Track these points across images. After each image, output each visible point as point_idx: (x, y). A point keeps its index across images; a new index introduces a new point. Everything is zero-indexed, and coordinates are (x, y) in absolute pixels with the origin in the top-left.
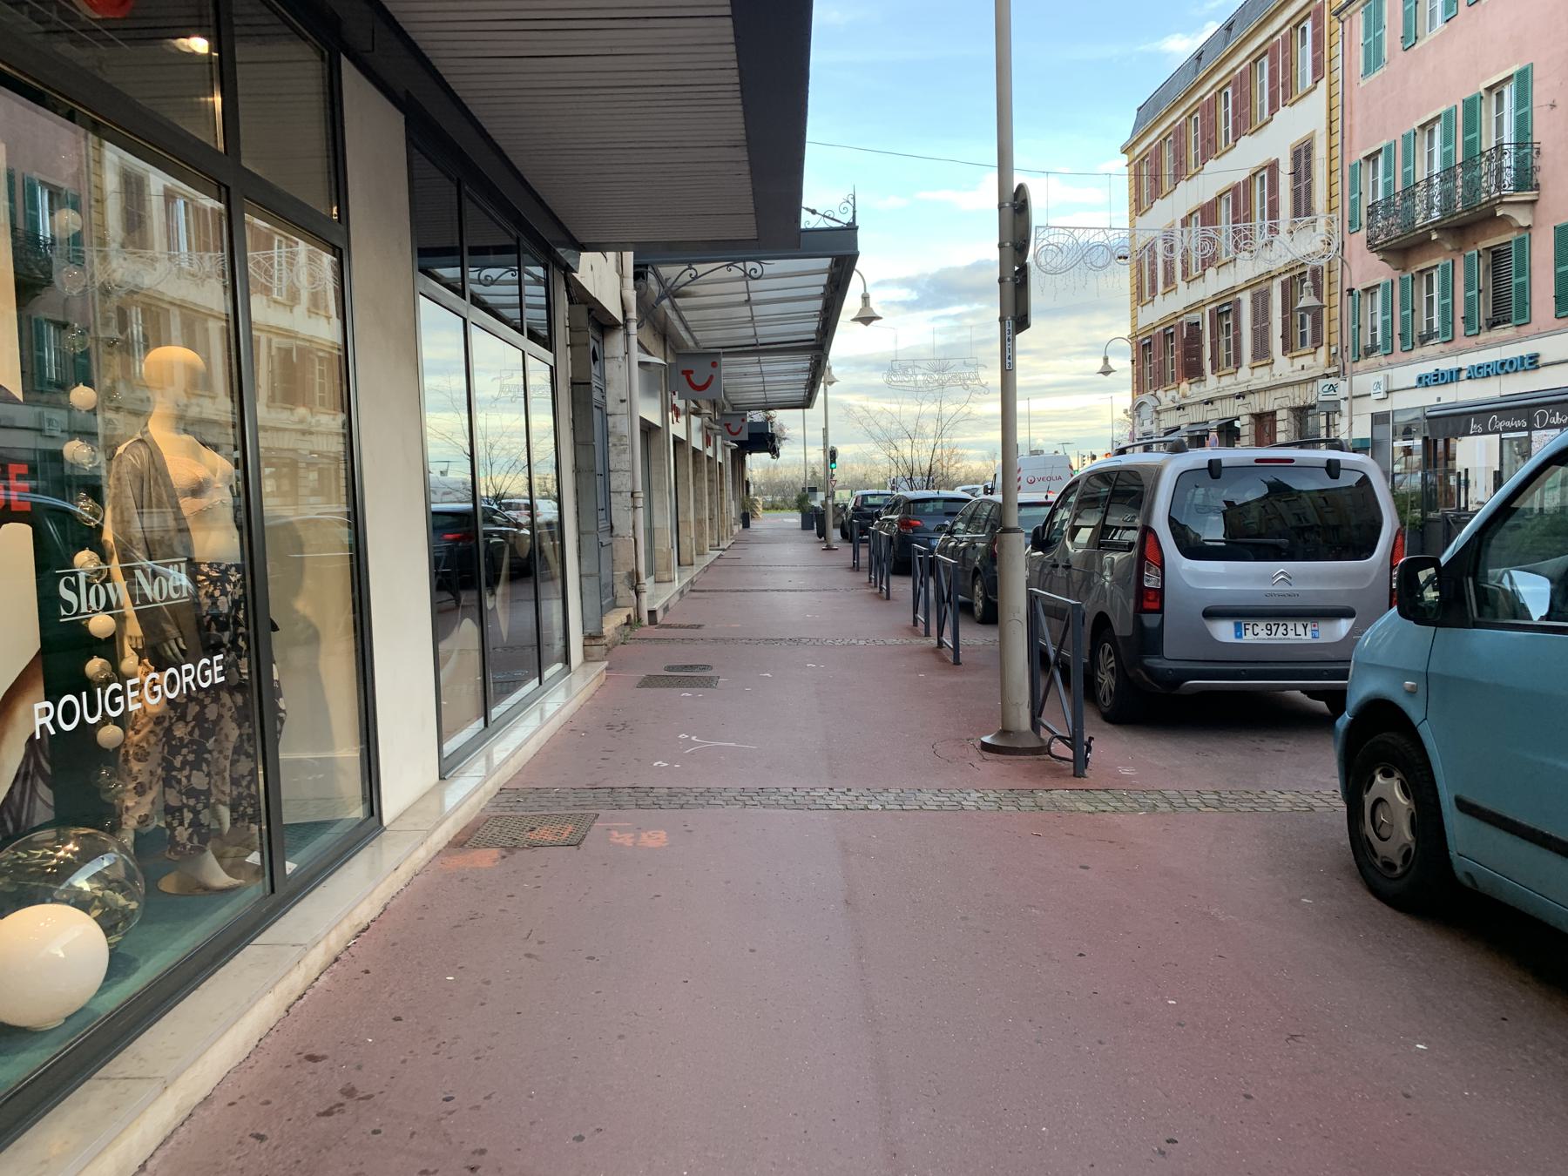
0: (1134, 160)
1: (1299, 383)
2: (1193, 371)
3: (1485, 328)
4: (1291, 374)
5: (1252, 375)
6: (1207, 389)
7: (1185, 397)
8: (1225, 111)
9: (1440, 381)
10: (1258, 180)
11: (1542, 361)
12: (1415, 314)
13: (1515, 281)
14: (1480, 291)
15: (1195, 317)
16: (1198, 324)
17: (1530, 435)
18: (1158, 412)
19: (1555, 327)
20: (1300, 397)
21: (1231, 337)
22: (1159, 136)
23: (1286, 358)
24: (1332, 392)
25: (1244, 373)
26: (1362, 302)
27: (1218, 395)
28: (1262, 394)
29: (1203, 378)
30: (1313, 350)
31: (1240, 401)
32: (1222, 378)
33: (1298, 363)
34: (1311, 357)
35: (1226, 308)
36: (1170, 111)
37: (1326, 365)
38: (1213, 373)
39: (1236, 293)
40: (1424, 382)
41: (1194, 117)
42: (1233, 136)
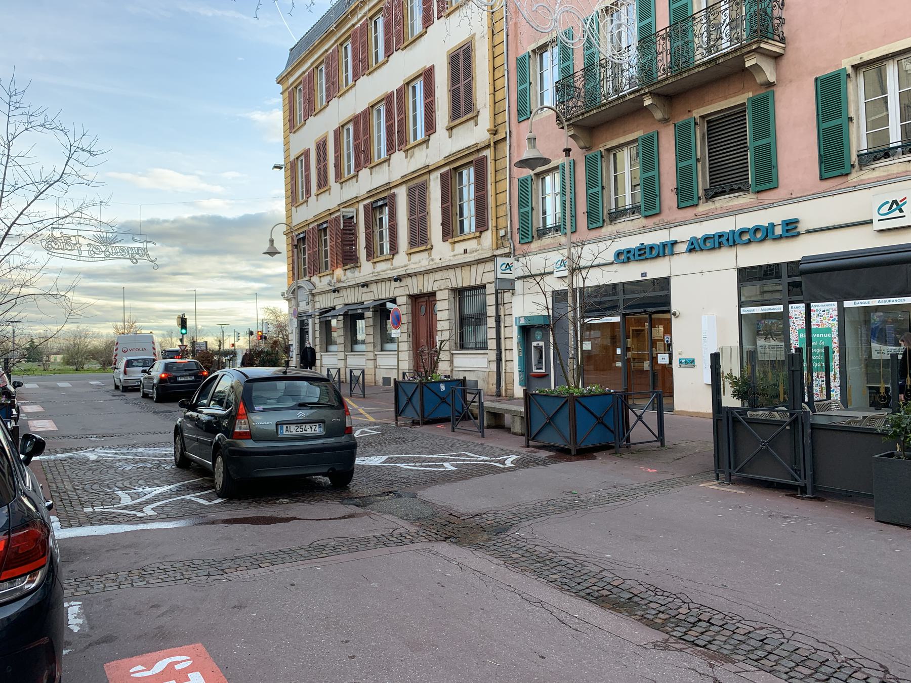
0: (288, 88)
1: (462, 265)
2: (349, 259)
3: (607, 221)
4: (452, 258)
5: (409, 260)
6: (361, 274)
7: (339, 281)
8: (321, 82)
9: (648, 255)
10: (375, 113)
11: (802, 228)
12: (604, 191)
13: (324, 260)
14: (698, 160)
15: (350, 212)
16: (352, 217)
17: (786, 309)
18: (313, 295)
19: (819, 190)
20: (416, 286)
21: (328, 248)
22: (312, 64)
23: (447, 243)
24: (508, 271)
25: (401, 259)
26: (534, 186)
27: (374, 278)
28: (420, 278)
29: (359, 265)
30: (478, 234)
31: (397, 284)
32: (377, 264)
33: (460, 248)
34: (475, 241)
35: (381, 203)
36: (322, 42)
37: (495, 247)
39: (390, 188)
40: (625, 257)
41: (298, 88)
42: (304, 117)
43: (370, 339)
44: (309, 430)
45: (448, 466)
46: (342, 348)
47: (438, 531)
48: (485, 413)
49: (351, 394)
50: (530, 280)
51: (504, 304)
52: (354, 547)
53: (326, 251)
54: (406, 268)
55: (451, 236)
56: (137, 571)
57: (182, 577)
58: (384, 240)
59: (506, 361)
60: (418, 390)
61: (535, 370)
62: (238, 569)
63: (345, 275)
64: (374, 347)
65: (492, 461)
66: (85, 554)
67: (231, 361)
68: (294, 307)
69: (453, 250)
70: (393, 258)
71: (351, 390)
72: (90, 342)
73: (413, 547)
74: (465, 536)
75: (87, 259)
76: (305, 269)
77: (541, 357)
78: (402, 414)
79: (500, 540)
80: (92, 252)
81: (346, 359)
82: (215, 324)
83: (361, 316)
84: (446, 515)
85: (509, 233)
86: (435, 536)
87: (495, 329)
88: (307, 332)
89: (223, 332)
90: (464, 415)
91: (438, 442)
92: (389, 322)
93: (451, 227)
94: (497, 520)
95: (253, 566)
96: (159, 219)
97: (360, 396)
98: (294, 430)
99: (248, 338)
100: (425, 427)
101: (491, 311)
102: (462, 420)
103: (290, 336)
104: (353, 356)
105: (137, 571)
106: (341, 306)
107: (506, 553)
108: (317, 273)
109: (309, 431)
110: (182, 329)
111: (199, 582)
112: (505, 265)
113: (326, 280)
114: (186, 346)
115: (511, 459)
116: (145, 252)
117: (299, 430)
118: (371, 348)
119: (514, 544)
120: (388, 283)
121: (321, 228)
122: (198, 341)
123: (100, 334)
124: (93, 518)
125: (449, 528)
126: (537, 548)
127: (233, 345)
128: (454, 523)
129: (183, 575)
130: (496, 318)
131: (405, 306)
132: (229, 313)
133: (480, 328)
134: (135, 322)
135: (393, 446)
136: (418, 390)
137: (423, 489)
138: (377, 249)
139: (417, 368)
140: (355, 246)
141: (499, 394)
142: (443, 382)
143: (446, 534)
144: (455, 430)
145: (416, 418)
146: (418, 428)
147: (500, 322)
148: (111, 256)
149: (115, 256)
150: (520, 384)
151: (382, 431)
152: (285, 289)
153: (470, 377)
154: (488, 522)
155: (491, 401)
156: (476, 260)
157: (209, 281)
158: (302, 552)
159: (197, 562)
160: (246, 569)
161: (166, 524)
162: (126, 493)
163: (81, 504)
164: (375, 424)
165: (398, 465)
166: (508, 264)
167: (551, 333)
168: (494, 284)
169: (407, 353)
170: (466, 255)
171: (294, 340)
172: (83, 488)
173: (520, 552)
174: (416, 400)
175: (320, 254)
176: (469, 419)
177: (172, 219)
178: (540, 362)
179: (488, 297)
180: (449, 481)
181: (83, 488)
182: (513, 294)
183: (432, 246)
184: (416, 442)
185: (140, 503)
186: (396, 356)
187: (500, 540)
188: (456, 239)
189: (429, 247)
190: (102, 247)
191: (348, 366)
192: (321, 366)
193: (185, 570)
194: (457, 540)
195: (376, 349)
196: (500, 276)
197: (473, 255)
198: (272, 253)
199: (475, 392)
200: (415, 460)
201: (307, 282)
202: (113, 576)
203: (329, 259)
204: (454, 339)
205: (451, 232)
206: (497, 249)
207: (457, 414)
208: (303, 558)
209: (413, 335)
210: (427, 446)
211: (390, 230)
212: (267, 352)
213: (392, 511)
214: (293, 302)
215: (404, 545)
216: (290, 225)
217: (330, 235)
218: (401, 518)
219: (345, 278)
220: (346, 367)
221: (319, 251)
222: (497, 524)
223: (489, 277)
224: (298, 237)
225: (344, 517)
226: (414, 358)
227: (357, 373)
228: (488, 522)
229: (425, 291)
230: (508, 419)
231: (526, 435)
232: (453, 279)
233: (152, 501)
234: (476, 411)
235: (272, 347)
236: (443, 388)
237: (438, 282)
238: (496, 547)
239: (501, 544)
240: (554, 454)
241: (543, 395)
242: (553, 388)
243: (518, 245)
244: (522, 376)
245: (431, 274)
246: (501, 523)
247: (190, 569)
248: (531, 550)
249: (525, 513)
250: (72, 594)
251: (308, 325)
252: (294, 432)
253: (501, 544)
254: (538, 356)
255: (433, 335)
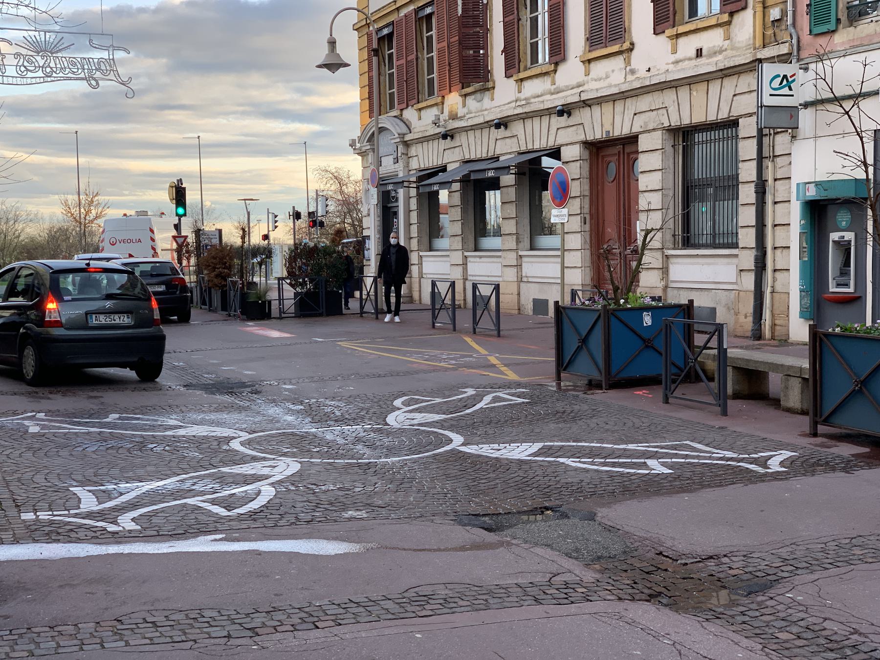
5: (587, 74)
6: (496, 103)
7: (454, 117)
13: (426, 77)
18: (407, 144)
21: (434, 54)
23: (662, 38)
24: (786, 91)
27: (519, 111)
28: (607, 108)
29: (490, 85)
30: (725, 18)
31: (563, 120)
33: (687, 46)
34: (719, 33)
37: (759, 43)
38: (508, 76)
43: (509, 227)
44: (118, 320)
45: (656, 466)
46: (457, 243)
47: (635, 583)
48: (730, 370)
49: (474, 329)
50: (830, 107)
51: (774, 156)
52: (482, 602)
53: (430, 61)
54: (581, 89)
55: (671, 22)
56: (110, 623)
57: (184, 638)
58: (540, 35)
59: (775, 271)
60: (600, 324)
61: (833, 288)
62: (279, 629)
63: (464, 105)
64: (518, 241)
65: (742, 460)
66: (27, 590)
67: (263, 267)
68: (372, 167)
69: (674, 51)
70: (555, 71)
71: (475, 322)
72: (23, 230)
73: (587, 607)
74: (686, 595)
75: (15, 81)
76: (392, 95)
77: (847, 263)
78: (568, 369)
79: (754, 606)
80: (23, 69)
81: (465, 265)
82: (234, 199)
83: (494, 184)
84: (651, 555)
85: (790, 14)
86: (630, 591)
87: (753, 208)
88: (396, 214)
89: (249, 214)
90: (689, 372)
91: (636, 421)
92: (547, 195)
93: (671, 5)
94: (750, 569)
95: (305, 626)
96: (131, 7)
97: (492, 333)
98: (103, 320)
99: (292, 225)
100: (612, 393)
101: (748, 172)
102: (684, 381)
103: (364, 220)
104: (478, 260)
105: (110, 623)
106: (457, 165)
107: (767, 629)
108: (415, 101)
109: (117, 321)
110: (177, 208)
111: (213, 648)
112: (780, 79)
113: (430, 115)
114: (186, 237)
115: (780, 458)
116: (110, 66)
117: (108, 319)
118: (511, 243)
119: (782, 615)
120: (545, 120)
121: (421, 14)
122: (207, 229)
123: (40, 216)
124: (36, 530)
125: (657, 577)
126: (826, 624)
127: (266, 237)
128: (666, 570)
129: (185, 634)
130: (757, 186)
131: (578, 164)
132: (257, 177)
133: (724, 206)
134: (97, 194)
135: (552, 426)
136: (600, 324)
137: (608, 505)
138: (526, 53)
139: (597, 282)
140: (485, 48)
141: (757, 335)
142: (648, 308)
143: (650, 588)
144: (670, 400)
145: (596, 376)
146: (599, 396)
147: (764, 193)
148: (54, 75)
149: (61, 75)
150: (802, 315)
151: (531, 397)
152: (356, 133)
153: (701, 302)
154: (731, 572)
155: (741, 348)
156: (721, 70)
157: (222, 121)
158: (389, 605)
159: (207, 613)
160: (292, 629)
161: (157, 545)
162: (90, 491)
163: (17, 506)
164: (519, 385)
165: (561, 460)
166: (785, 77)
167: (870, 212)
168: (754, 118)
169: (579, 253)
170: (699, 60)
171: (371, 227)
172: (19, 480)
173: (795, 629)
174: (597, 342)
175: (420, 66)
176: (698, 379)
177: (152, 8)
178: (844, 271)
179: (742, 144)
180: (658, 493)
181: (19, 480)
182: (793, 137)
183: (632, 44)
184: (594, 420)
185: (113, 509)
186: (559, 260)
187: (754, 606)
188: (682, 29)
189: (627, 45)
190: (39, 58)
191: (469, 278)
192: (421, 276)
193: (188, 627)
194: (671, 601)
195: (521, 245)
196: (768, 101)
197: (715, 59)
198: (334, 65)
199: (711, 329)
200: (592, 454)
201: (396, 119)
202: (70, 629)
203: (435, 75)
204: (672, 226)
205: (671, 16)
206: (764, 47)
207: (674, 370)
208: (391, 616)
209: (591, 219)
210: (616, 428)
211: (550, 16)
212: (325, 248)
213: (549, 542)
214: (370, 158)
215: (572, 603)
216: (365, 11)
217: (438, 29)
218: (566, 555)
219: (465, 110)
220: (465, 280)
221: (417, 59)
222: (748, 576)
223: (747, 104)
224: (380, 35)
225: (462, 549)
226: (592, 263)
227: (485, 291)
228: (731, 572)
229: (617, 133)
230: (775, 382)
231: (811, 413)
232: (673, 110)
233: (132, 505)
234: (712, 365)
235: (333, 241)
236: (647, 320)
237: (643, 116)
238: (747, 618)
239: (757, 614)
240: (867, 450)
241: (847, 337)
242: (869, 323)
243: (806, 38)
244: (807, 301)
245: (629, 101)
246: (758, 574)
247: (197, 625)
248: (817, 628)
249: (805, 559)
250: (7, 654)
251: (397, 200)
252: (104, 322)
253: (757, 614)
254: (839, 264)
255: (630, 220)
